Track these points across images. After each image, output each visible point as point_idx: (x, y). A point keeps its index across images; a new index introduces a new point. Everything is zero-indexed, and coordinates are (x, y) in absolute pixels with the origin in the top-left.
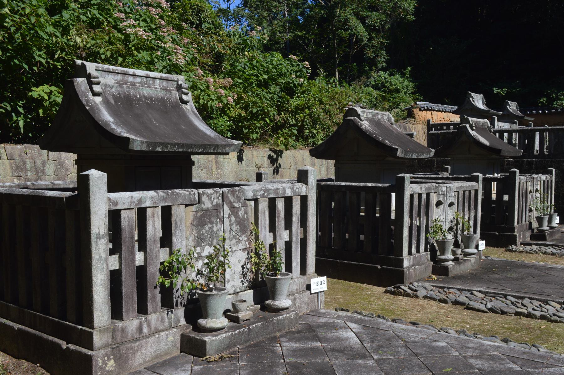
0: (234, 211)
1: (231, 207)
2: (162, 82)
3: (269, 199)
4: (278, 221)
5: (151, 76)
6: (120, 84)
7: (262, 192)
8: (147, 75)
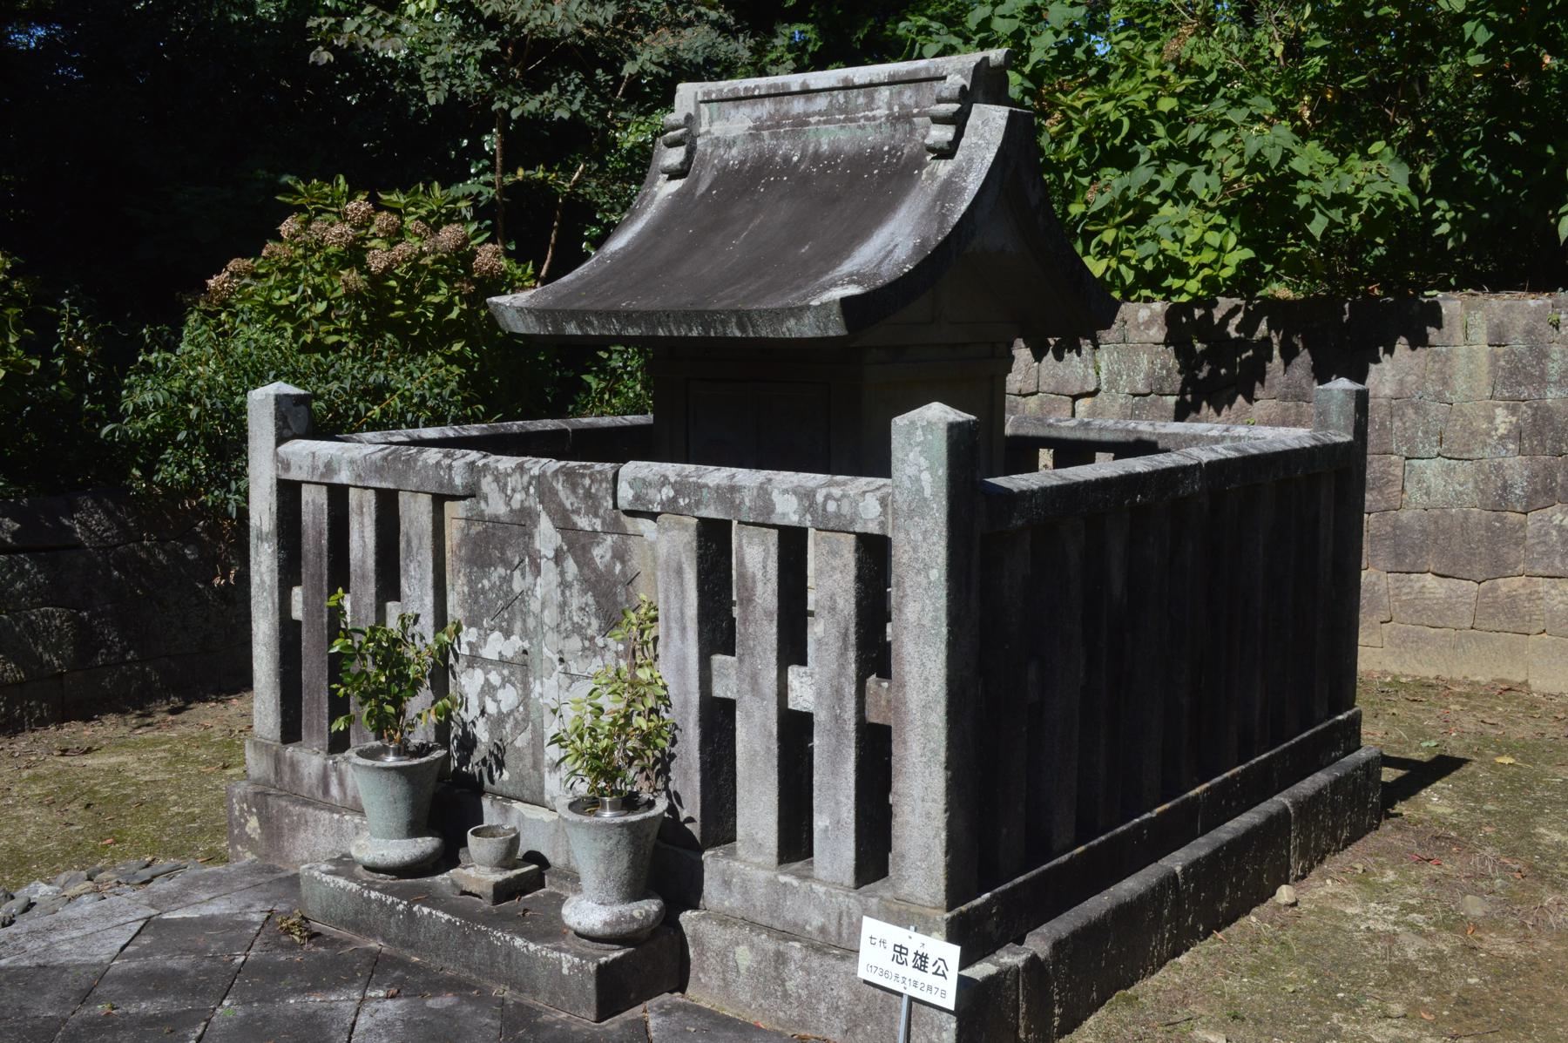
0: (576, 543)
1: (565, 526)
2: (900, 93)
4: (745, 620)
5: (857, 81)
7: (668, 492)
8: (846, 80)
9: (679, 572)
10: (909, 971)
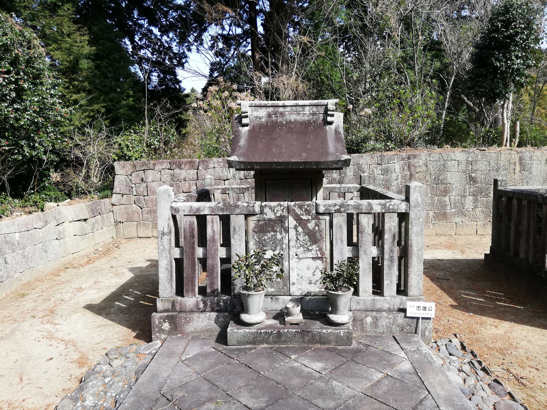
1: (298, 218)
2: (312, 108)
3: (347, 213)
6: (269, 115)
9: (341, 226)
10: (422, 311)
